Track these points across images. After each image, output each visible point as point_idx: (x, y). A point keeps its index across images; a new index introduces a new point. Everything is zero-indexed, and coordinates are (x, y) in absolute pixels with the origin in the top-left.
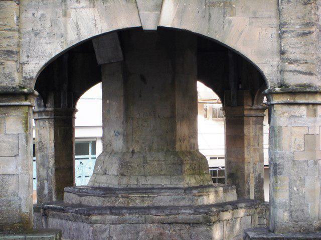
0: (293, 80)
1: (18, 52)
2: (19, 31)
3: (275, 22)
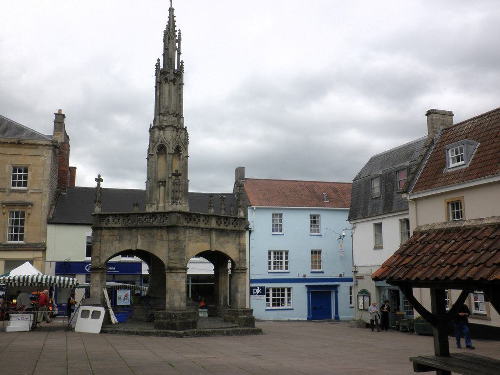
0: (171, 265)
1: (100, 257)
2: (100, 250)
3: (167, 248)
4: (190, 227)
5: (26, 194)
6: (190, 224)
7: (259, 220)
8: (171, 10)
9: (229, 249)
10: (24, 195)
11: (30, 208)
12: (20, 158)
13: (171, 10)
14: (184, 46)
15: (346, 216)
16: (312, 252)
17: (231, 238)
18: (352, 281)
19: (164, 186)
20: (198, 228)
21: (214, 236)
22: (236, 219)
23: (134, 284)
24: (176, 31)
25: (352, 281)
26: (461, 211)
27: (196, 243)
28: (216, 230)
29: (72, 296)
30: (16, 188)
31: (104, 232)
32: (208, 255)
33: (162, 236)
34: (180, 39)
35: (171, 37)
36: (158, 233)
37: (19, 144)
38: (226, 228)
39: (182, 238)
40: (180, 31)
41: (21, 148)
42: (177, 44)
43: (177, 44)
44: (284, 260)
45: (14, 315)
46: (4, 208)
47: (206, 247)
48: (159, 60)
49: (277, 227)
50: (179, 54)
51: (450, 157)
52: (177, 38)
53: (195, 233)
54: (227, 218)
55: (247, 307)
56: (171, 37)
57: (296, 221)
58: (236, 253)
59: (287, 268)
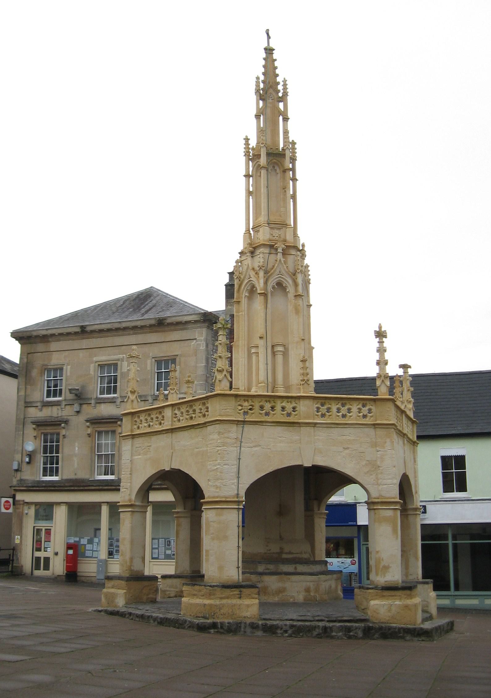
5: (59, 407)
8: (269, 51)
10: (55, 408)
11: (64, 428)
12: (164, 346)
13: (269, 51)
14: (295, 106)
16: (119, 490)
18: (460, 461)
24: (278, 83)
25: (460, 461)
29: (376, 447)
30: (52, 399)
34: (285, 94)
35: (271, 95)
37: (161, 324)
40: (285, 81)
41: (164, 331)
42: (281, 105)
43: (281, 105)
45: (241, 516)
46: (88, 427)
48: (247, 140)
50: (286, 119)
52: (280, 95)
56: (271, 95)
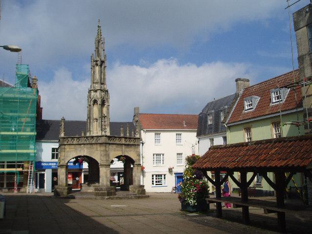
4: (111, 144)
6: (111, 142)
7: (147, 137)
9: (132, 154)
15: (195, 134)
17: (132, 148)
19: (97, 121)
20: (115, 144)
21: (124, 148)
22: (135, 139)
23: (23, 167)
26: (8, 162)
27: (115, 152)
28: (125, 145)
31: (66, 147)
32: (119, 158)
33: (97, 148)
36: (95, 146)
38: (130, 143)
39: (107, 149)
44: (162, 159)
47: (120, 154)
49: (157, 141)
51: (274, 96)
53: (114, 146)
54: (130, 138)
55: (142, 184)
57: (168, 137)
58: (136, 155)
59: (163, 163)
